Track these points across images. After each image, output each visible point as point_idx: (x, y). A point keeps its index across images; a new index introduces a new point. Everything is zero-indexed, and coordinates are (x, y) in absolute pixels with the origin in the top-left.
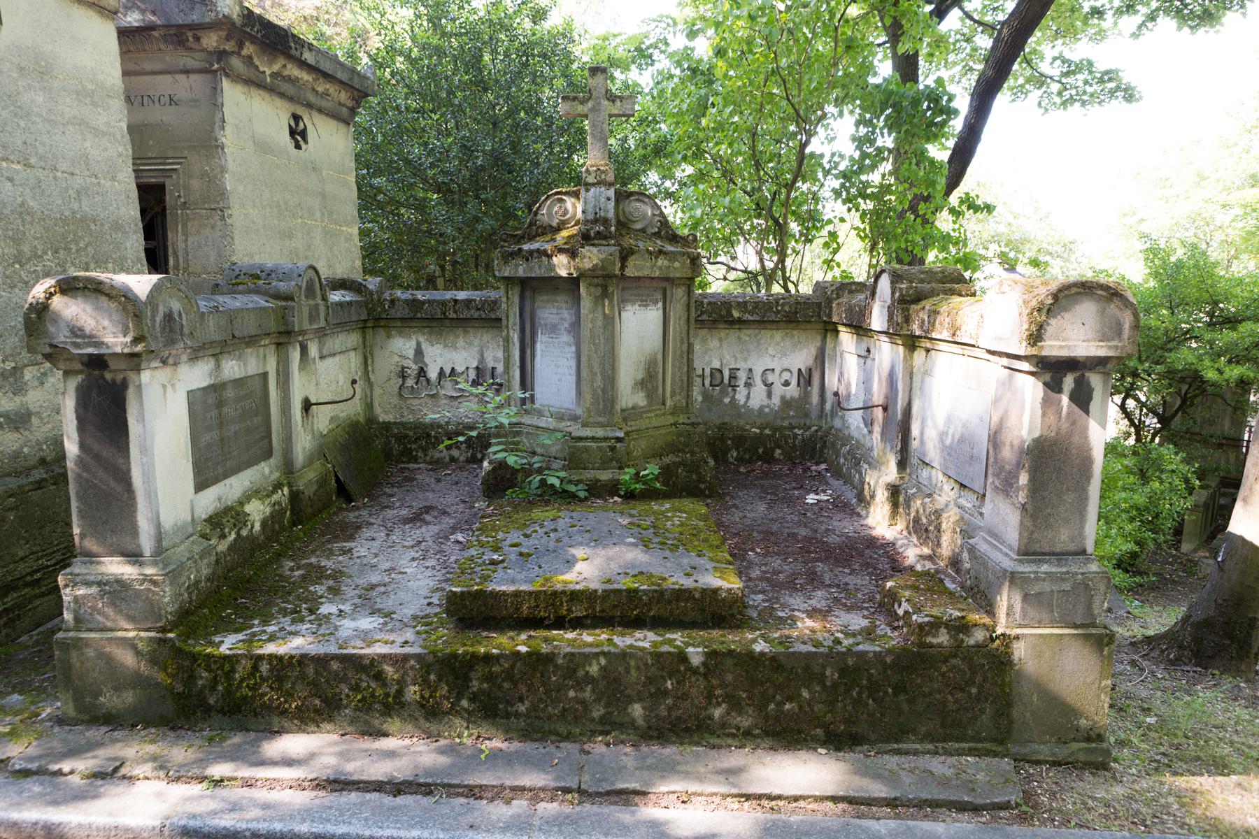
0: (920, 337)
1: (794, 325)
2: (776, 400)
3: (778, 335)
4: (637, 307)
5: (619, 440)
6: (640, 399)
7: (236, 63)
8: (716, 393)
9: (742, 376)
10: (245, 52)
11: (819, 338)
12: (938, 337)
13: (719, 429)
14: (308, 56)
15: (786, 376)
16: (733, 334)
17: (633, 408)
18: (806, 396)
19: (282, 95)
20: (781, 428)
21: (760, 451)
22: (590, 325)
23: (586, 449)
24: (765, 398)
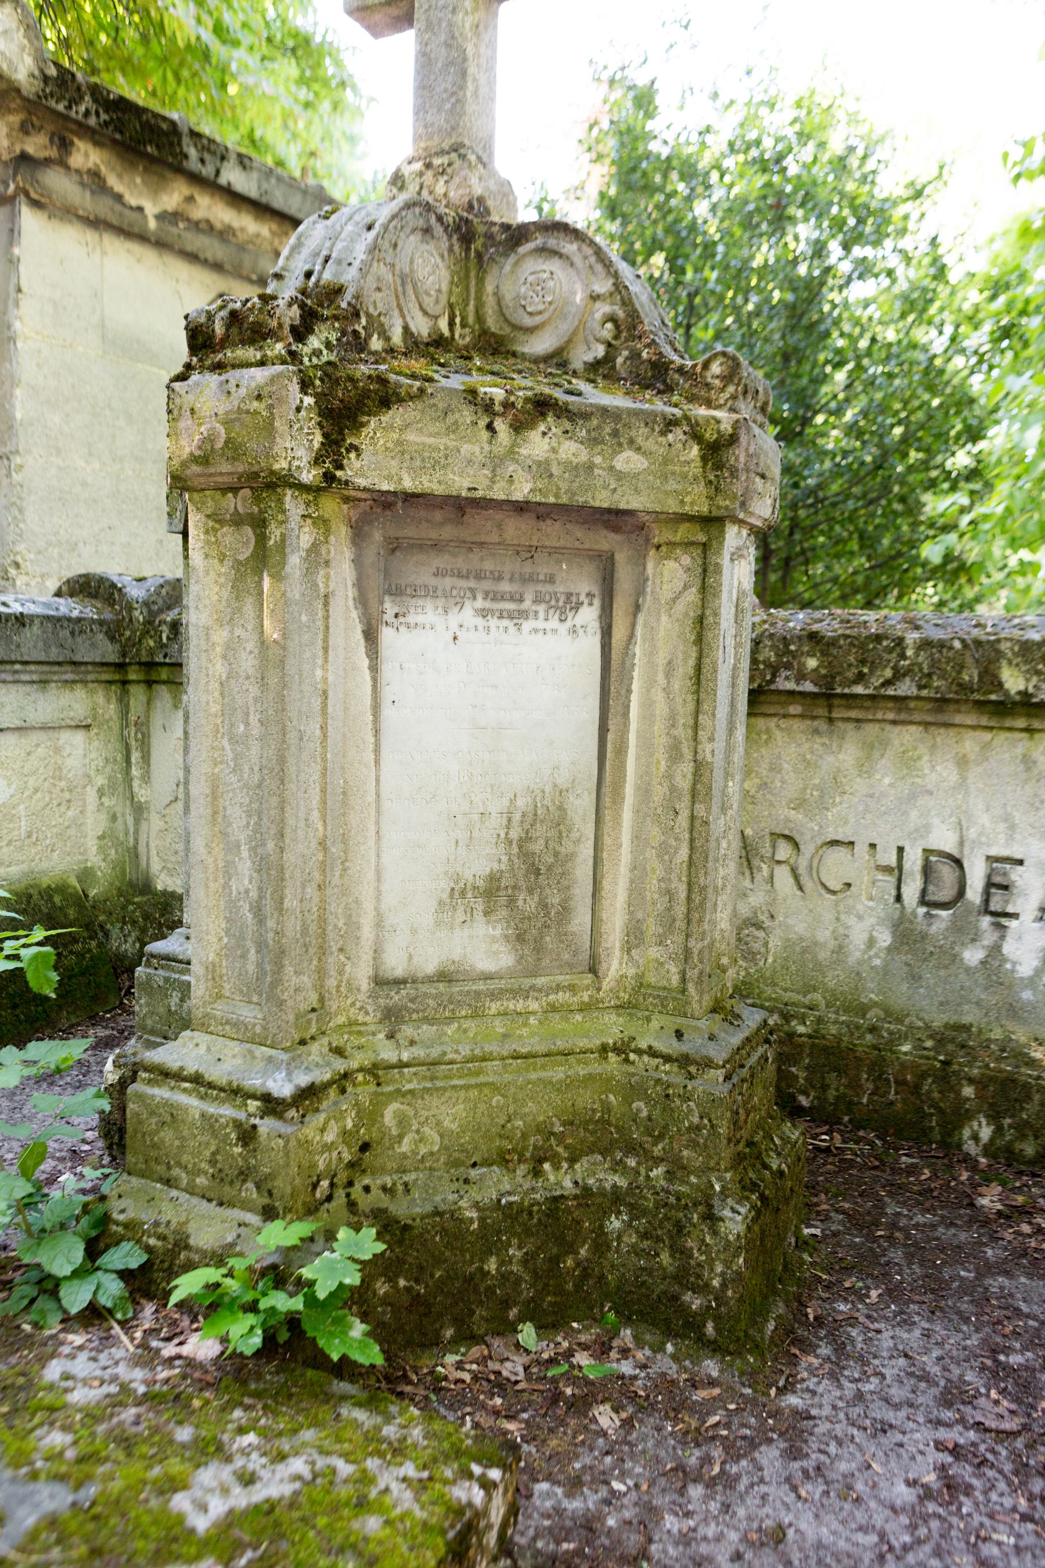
4: (468, 614)
5: (272, 1105)
6: (482, 947)
7: (55, 180)
10: (77, 160)
13: (941, 1041)
14: (232, 176)
16: (1007, 748)
17: (444, 976)
19: (192, 257)
22: (219, 668)
23: (173, 1116)
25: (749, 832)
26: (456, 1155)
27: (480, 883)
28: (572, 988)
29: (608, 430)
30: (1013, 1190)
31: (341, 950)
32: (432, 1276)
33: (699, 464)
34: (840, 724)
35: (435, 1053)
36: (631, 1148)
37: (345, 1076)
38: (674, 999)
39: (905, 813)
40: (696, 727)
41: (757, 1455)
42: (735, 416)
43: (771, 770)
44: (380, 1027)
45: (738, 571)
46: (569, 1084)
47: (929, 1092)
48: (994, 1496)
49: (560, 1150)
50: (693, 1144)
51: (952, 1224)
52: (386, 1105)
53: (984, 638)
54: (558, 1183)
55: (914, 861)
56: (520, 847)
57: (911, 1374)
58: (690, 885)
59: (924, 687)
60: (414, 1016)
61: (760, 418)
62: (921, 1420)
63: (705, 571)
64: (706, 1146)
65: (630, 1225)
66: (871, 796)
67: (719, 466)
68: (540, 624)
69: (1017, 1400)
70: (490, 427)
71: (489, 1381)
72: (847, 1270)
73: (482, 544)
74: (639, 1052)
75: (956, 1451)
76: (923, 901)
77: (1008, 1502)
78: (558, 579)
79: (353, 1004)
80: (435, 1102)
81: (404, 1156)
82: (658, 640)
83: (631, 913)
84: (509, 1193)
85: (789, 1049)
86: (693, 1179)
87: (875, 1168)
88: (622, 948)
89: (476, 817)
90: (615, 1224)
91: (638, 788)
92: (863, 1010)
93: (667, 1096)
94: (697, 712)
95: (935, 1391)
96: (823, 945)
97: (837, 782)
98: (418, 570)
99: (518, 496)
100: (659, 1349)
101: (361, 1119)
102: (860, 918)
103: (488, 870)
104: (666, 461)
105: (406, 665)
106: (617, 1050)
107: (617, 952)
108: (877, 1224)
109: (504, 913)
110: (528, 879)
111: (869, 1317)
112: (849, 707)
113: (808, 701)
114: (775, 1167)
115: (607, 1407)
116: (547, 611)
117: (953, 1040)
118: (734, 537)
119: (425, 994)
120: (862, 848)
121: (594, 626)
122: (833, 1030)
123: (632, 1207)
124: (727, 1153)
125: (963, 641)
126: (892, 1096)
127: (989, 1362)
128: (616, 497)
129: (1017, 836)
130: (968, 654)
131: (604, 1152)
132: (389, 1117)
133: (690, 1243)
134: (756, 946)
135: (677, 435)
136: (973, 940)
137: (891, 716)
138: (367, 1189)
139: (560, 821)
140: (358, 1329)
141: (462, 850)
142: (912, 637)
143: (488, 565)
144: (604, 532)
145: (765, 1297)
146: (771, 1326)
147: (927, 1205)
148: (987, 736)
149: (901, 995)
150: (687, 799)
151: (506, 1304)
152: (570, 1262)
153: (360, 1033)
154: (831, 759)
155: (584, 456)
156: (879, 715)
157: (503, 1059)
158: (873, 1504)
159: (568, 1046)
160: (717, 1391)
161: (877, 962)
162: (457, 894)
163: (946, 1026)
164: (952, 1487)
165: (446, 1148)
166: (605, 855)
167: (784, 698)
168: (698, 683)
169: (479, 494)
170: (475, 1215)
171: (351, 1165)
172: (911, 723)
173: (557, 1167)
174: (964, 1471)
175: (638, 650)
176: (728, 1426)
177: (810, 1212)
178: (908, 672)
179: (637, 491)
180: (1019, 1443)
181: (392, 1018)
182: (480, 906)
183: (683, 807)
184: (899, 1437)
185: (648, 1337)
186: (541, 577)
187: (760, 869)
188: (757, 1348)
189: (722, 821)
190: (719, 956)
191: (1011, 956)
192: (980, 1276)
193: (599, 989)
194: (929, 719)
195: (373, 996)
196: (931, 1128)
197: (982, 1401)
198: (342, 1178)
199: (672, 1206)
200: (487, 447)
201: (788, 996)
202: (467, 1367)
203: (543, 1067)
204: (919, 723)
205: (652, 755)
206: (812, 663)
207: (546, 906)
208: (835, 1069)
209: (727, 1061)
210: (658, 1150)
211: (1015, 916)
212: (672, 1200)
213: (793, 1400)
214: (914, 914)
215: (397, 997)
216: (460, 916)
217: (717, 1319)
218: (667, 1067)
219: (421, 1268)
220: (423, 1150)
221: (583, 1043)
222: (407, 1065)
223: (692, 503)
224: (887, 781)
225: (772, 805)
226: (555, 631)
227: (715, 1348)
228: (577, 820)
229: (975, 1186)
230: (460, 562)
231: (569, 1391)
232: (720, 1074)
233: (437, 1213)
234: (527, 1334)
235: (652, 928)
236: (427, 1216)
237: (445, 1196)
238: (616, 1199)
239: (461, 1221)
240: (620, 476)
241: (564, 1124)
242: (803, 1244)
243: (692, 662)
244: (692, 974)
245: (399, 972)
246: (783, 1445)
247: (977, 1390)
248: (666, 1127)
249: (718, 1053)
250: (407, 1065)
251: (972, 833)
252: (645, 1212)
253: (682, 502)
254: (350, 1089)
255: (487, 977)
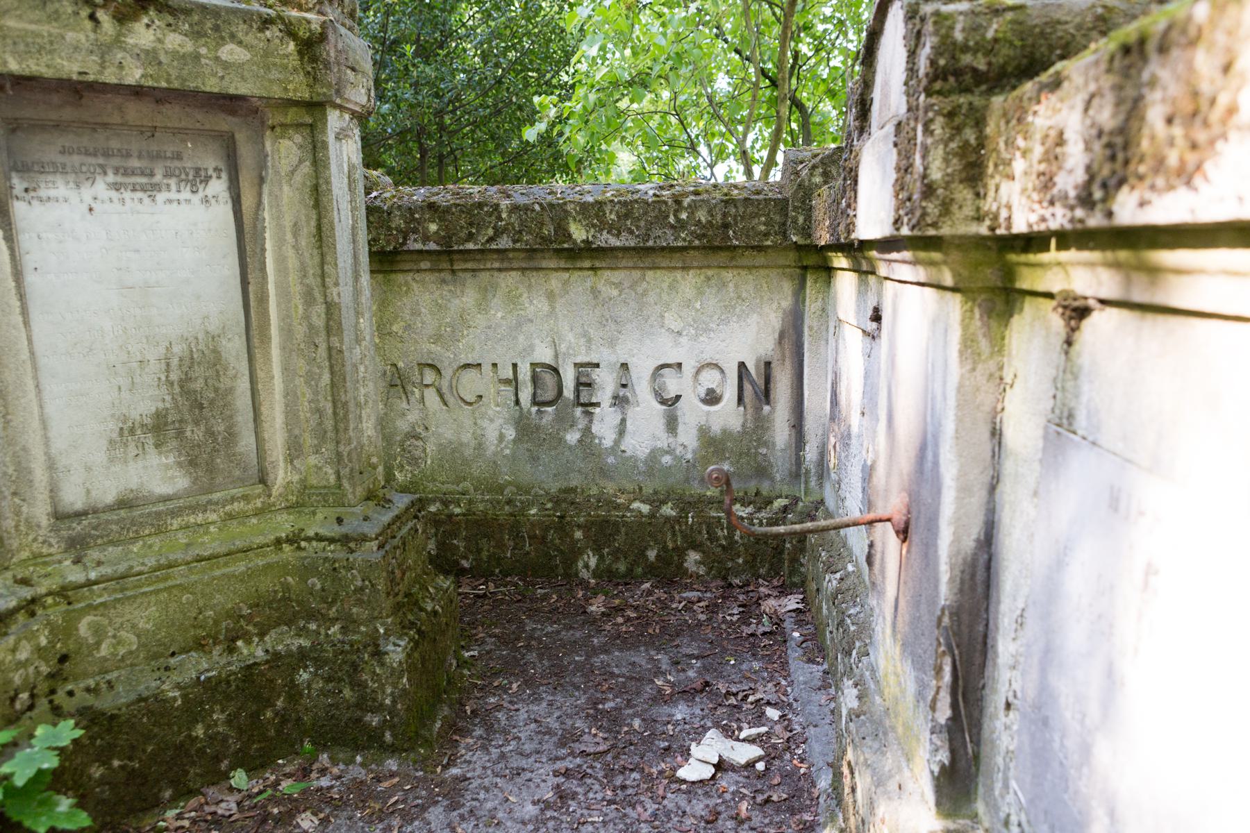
0: (1033, 242)
1: (722, 257)
2: (688, 438)
3: (688, 282)
4: (100, 187)
6: (158, 474)
8: (547, 419)
9: (606, 382)
11: (787, 287)
12: (1169, 209)
13: (557, 502)
15: (710, 379)
16: (580, 283)
17: (124, 503)
18: (759, 427)
20: (699, 503)
21: (652, 554)
24: (1054, 303)
25: (401, 364)
26: (155, 649)
27: (148, 421)
28: (245, 498)
29: (209, 25)
30: (613, 597)
31: (15, 494)
32: (144, 751)
33: (297, 57)
34: (460, 274)
35: (122, 568)
36: (311, 615)
37: (33, 601)
38: (333, 494)
39: (515, 338)
40: (323, 276)
41: (426, 815)
42: (323, 18)
43: (413, 314)
44: (66, 555)
45: (345, 151)
46: (251, 574)
47: (552, 541)
48: (591, 795)
49: (250, 628)
50: (360, 602)
51: (572, 628)
52: (79, 620)
53: (555, 202)
54: (251, 655)
55: (525, 373)
56: (182, 387)
57: (539, 732)
58: (334, 402)
59: (518, 241)
60: (99, 541)
61: (348, 22)
62: (544, 760)
63: (314, 147)
64: (369, 602)
65: (316, 674)
66: (489, 327)
67: (314, 60)
68: (173, 195)
69: (609, 731)
70: (92, 17)
71: (206, 821)
72: (496, 674)
73: (105, 125)
74: (309, 539)
75: (567, 774)
76: (535, 402)
77: (599, 796)
78: (185, 156)
79: (35, 540)
80: (128, 609)
81: (105, 659)
82: (281, 207)
83: (289, 431)
84: (207, 670)
85: (444, 526)
86: (363, 629)
87: (519, 601)
88: (285, 460)
89: (135, 365)
90: (304, 676)
91: (281, 329)
92: (501, 489)
93: (335, 569)
94: (322, 263)
95: (555, 739)
96: (467, 445)
97: (463, 320)
98: (46, 149)
99: (130, 81)
100: (351, 761)
101: (55, 635)
102: (492, 420)
103: (153, 409)
104: (266, 54)
105: (43, 235)
106: (290, 541)
107: (282, 464)
108: (518, 639)
109: (174, 443)
110: (192, 410)
111: (510, 702)
112: (466, 261)
113: (434, 258)
114: (429, 609)
115: (308, 813)
116: (178, 184)
117: (565, 500)
118: (335, 120)
119: (108, 522)
120: (487, 368)
121: (225, 196)
122: (481, 507)
123: (316, 660)
124: (388, 604)
125: (541, 205)
126: (527, 548)
127: (591, 711)
128: (225, 83)
129: (593, 347)
130: (545, 214)
131: (289, 623)
132: (84, 628)
133: (364, 677)
134: (417, 453)
135: (273, 32)
136: (572, 426)
137: (497, 265)
138: (71, 694)
139: (216, 361)
140: (65, 804)
141: (125, 394)
142: (505, 203)
143: (115, 144)
144: (223, 115)
145: (434, 706)
146: (438, 725)
147: (555, 619)
148: (566, 275)
149: (526, 473)
150: (323, 334)
151: (217, 759)
152: (269, 714)
153: (45, 564)
154: (457, 301)
155: (189, 46)
156: (488, 266)
157: (188, 563)
158: (509, 824)
159: (247, 544)
160: (397, 779)
161: (507, 452)
162: (126, 432)
163: (560, 491)
164: (563, 796)
165: (144, 645)
166: (260, 386)
167: (415, 257)
168: (320, 239)
169: (91, 78)
170: (177, 694)
171: (51, 676)
172: (512, 269)
173: (248, 642)
174: (573, 785)
175: (266, 215)
176: (404, 801)
177: (471, 640)
178: (505, 230)
179: (243, 79)
180: (609, 758)
181: (77, 547)
182: (150, 440)
183: (321, 340)
184: (529, 775)
185: (341, 756)
186: (169, 154)
187: (413, 393)
188: (428, 743)
189: (358, 350)
190: (369, 457)
191: (598, 434)
192: (588, 657)
193: (270, 496)
194: (524, 265)
195: (54, 529)
196: (557, 566)
197: (586, 737)
198: (43, 687)
199: (348, 652)
200: (92, 36)
201: (445, 488)
202: (187, 816)
203: (226, 564)
204: (517, 269)
205: (289, 302)
206: (433, 227)
207: (213, 433)
208: (485, 536)
209: (380, 535)
210: (332, 613)
211: (597, 405)
212: (347, 647)
213: (455, 771)
214: (529, 412)
215: (78, 528)
216: (132, 451)
217: (392, 727)
218: (332, 547)
219: (133, 747)
220: (122, 651)
221: (259, 540)
222: (96, 583)
223: (295, 90)
224: (499, 315)
225: (416, 342)
226: (188, 201)
227: (393, 750)
228: (232, 360)
229: (587, 599)
230: (85, 141)
231: (276, 811)
232: (374, 545)
233: (141, 699)
234: (239, 778)
235: (308, 440)
236: (132, 703)
237: (148, 683)
238: (302, 656)
239: (165, 701)
240: (226, 65)
241: (250, 607)
242: (462, 663)
243: (313, 223)
244: (345, 472)
245: (79, 506)
246: (446, 803)
247: (583, 731)
248: (337, 594)
249: (371, 529)
250: (96, 583)
251: (563, 348)
252: (326, 662)
253: (286, 89)
254: (40, 612)
255: (166, 499)
